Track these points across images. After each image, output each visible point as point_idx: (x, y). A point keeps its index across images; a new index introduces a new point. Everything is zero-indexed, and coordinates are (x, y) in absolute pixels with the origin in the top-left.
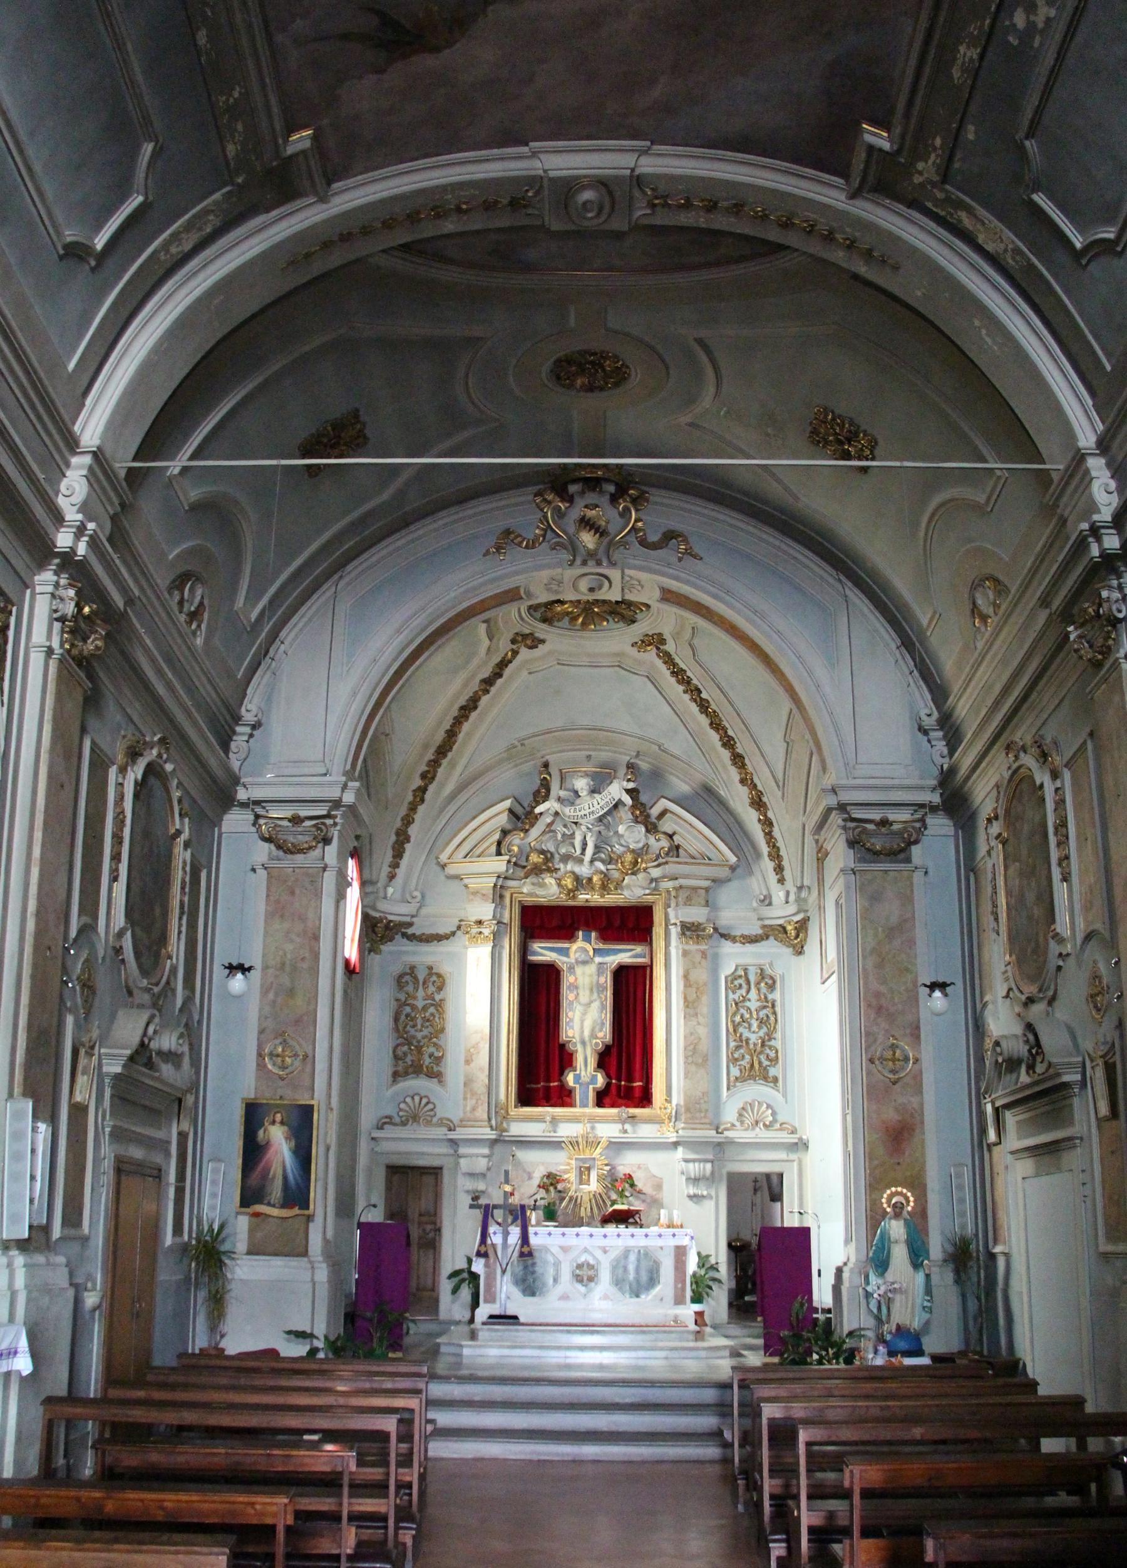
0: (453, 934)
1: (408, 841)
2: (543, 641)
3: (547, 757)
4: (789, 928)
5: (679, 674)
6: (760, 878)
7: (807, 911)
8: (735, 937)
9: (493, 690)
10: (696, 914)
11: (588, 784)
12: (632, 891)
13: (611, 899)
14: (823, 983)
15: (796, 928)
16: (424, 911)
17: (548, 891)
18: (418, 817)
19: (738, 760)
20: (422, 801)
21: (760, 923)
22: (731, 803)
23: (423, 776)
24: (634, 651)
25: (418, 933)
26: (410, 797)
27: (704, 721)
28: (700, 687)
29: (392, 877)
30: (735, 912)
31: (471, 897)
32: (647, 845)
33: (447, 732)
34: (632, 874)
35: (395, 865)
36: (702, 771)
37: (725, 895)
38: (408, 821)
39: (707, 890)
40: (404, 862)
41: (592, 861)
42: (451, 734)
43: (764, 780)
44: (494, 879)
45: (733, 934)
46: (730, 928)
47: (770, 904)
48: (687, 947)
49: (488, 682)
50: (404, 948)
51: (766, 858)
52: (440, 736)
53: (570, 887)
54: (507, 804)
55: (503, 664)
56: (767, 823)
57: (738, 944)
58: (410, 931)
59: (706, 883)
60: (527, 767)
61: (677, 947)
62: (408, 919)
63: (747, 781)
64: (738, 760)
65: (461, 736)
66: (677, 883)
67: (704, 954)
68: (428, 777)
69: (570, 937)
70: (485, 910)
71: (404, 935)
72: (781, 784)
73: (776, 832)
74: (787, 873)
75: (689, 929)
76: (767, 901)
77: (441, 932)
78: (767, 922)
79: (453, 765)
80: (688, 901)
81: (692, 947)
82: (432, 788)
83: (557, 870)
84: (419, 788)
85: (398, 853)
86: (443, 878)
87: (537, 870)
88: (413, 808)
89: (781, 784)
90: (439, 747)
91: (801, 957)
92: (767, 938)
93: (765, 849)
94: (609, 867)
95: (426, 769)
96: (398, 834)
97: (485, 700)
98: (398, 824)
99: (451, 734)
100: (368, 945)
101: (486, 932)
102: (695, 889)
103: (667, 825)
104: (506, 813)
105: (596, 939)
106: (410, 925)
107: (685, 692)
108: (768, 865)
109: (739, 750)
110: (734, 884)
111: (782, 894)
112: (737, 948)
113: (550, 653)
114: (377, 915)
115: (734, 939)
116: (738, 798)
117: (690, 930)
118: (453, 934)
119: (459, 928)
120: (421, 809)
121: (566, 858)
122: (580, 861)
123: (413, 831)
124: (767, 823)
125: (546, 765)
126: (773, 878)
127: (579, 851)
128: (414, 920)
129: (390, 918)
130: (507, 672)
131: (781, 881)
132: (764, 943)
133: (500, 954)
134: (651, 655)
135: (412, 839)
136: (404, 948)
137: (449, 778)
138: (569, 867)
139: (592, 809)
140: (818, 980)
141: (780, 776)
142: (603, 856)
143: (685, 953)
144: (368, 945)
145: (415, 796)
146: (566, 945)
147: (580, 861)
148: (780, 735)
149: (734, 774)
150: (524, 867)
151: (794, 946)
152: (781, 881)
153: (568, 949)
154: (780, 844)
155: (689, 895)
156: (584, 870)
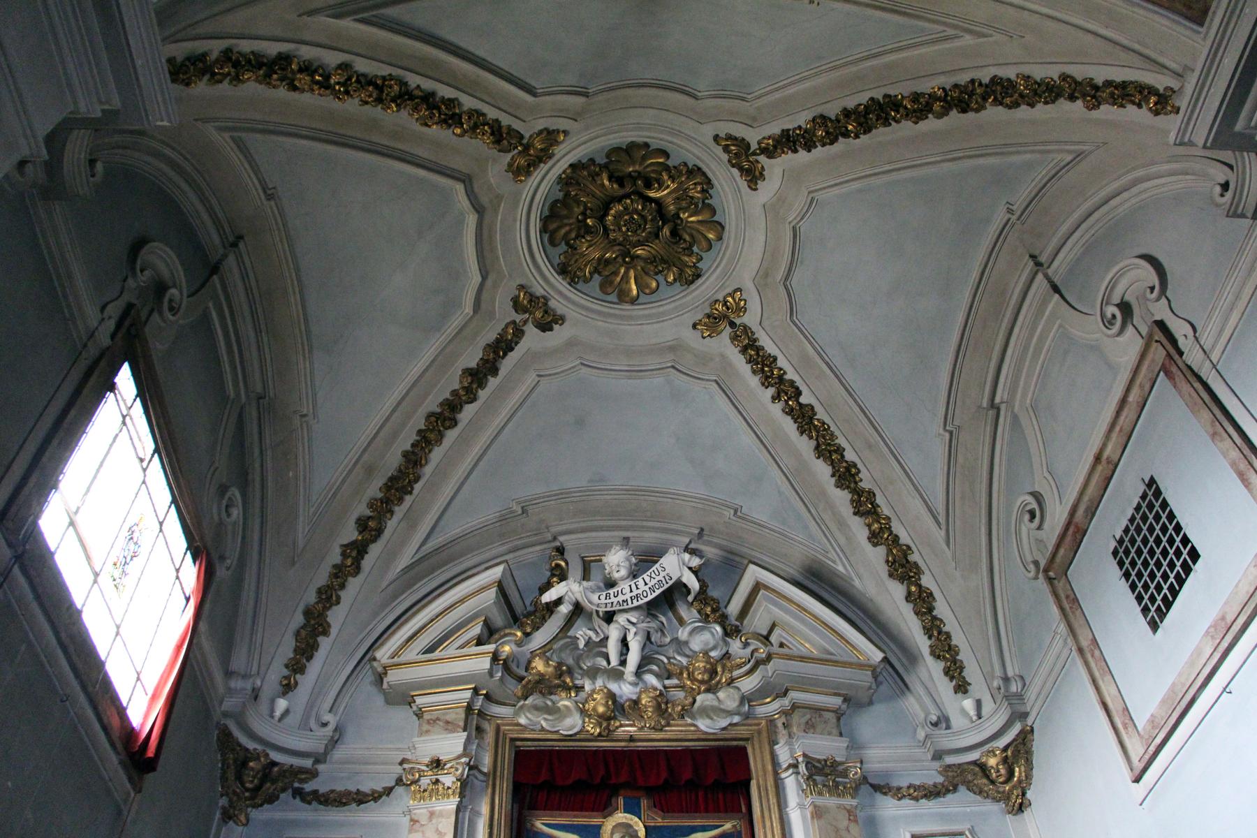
0: (388, 791)
1: (326, 633)
2: (560, 320)
3: (562, 539)
4: (992, 762)
5: (763, 364)
6: (921, 691)
7: (1025, 715)
8: (899, 789)
9: (483, 394)
10: (826, 746)
11: (628, 559)
12: (710, 719)
13: (676, 734)
14: (1137, 780)
15: (1005, 760)
16: (339, 753)
17: (566, 721)
18: (347, 595)
19: (865, 505)
20: (357, 569)
21: (936, 765)
22: (857, 583)
23: (362, 524)
24: (692, 339)
25: (323, 789)
26: (335, 557)
27: (805, 445)
28: (799, 383)
29: (288, 688)
30: (887, 745)
31: (426, 727)
32: (727, 656)
33: (406, 455)
34: (708, 691)
35: (296, 667)
36: (806, 542)
37: (868, 724)
38: (328, 596)
39: (839, 715)
40: (314, 668)
41: (639, 673)
42: (414, 459)
43: (913, 524)
44: (468, 694)
45: (895, 784)
46: (887, 774)
47: (948, 727)
48: (820, 801)
49: (478, 376)
50: (292, 815)
51: (930, 660)
52: (393, 461)
53: (601, 709)
54: (497, 572)
55: (503, 346)
56: (922, 601)
57: (906, 801)
58: (308, 787)
59: (836, 701)
60: (532, 554)
61: (801, 806)
62: (308, 763)
63: (881, 534)
64: (865, 505)
65: (428, 470)
66: (786, 702)
67: (851, 814)
68: (370, 529)
69: (605, 808)
70: (451, 745)
71: (298, 793)
72: (942, 519)
73: (941, 609)
74: (972, 673)
75: (820, 771)
76: (942, 722)
77: (366, 788)
78: (950, 760)
79: (411, 522)
80: (809, 727)
81: (829, 801)
82: (375, 550)
83: (579, 689)
84: (353, 544)
85: (306, 649)
86: (380, 700)
87: (543, 686)
88: (341, 574)
89: (942, 519)
90: (392, 479)
91: (1027, 813)
92: (955, 789)
93: (923, 643)
94: (667, 682)
95: (368, 513)
96: (308, 613)
97: (468, 413)
98: (311, 597)
99: (414, 459)
100: (223, 801)
101: (448, 780)
102: (818, 710)
103: (758, 620)
104: (494, 590)
105: (649, 808)
106: (313, 774)
107: (776, 398)
108: (933, 668)
109: (865, 485)
110: (878, 709)
111: (968, 704)
112: (906, 808)
113: (571, 344)
114: (251, 745)
115: (898, 793)
116: (867, 571)
117: (822, 773)
118: (388, 791)
119: (399, 781)
120: (354, 584)
121: (593, 673)
122: (617, 675)
123: (336, 616)
124: (922, 601)
125: (561, 551)
126: (944, 687)
127: (614, 661)
128: (321, 767)
129: (276, 756)
130: (508, 364)
131: (962, 688)
132: (950, 796)
133: (472, 825)
134: (724, 345)
135: (334, 631)
136: (292, 815)
137: (402, 544)
138: (599, 683)
139: (635, 592)
140: (1127, 776)
141: (940, 508)
142: (655, 668)
143: (818, 813)
144: (223, 801)
145: (344, 554)
146: (595, 821)
147: (617, 675)
148: (936, 426)
149: (859, 529)
150: (521, 679)
151: (1006, 797)
152: (962, 688)
153: (599, 827)
154: (951, 625)
155: (814, 717)
156: (625, 690)
